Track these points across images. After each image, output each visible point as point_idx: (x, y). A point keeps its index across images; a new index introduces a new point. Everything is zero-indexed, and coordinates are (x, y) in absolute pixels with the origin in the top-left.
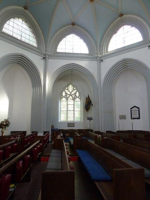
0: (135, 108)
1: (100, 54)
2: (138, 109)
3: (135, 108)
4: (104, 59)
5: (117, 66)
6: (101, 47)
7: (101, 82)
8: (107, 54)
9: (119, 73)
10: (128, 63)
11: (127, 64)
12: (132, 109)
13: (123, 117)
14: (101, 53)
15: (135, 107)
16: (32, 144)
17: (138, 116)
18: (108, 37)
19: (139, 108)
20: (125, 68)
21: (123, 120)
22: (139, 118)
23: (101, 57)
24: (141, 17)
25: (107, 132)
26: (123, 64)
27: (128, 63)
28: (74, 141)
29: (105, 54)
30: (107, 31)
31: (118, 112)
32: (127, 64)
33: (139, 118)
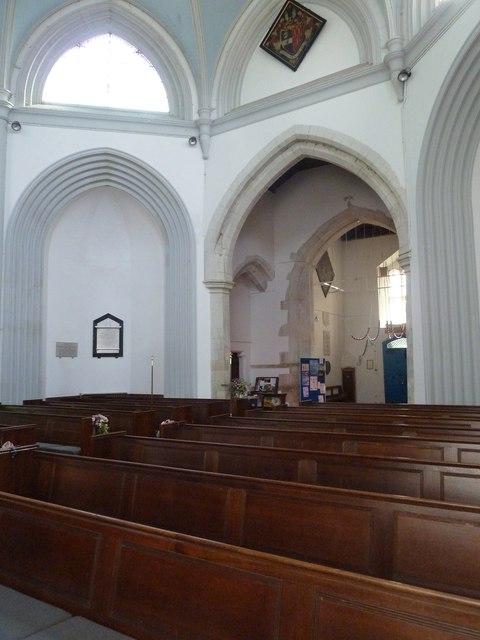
0: (108, 320)
1: (11, 95)
2: (117, 325)
3: (108, 322)
4: (28, 124)
5: (88, 160)
6: (16, 72)
7: (5, 215)
8: (35, 106)
9: (74, 194)
10: (118, 167)
11: (113, 175)
12: (99, 325)
13: (67, 350)
14: (19, 96)
15: (108, 316)
16: (410, 584)
17: (115, 349)
18: (50, 44)
19: (121, 322)
20: (100, 181)
21: (279, 306)
22: (120, 354)
23: (12, 111)
24: (174, 37)
25: (26, 402)
26: (92, 173)
27: (118, 167)
28: (190, 411)
29: (32, 106)
30: (49, 23)
31: (53, 336)
32: (112, 172)
33: (120, 354)
